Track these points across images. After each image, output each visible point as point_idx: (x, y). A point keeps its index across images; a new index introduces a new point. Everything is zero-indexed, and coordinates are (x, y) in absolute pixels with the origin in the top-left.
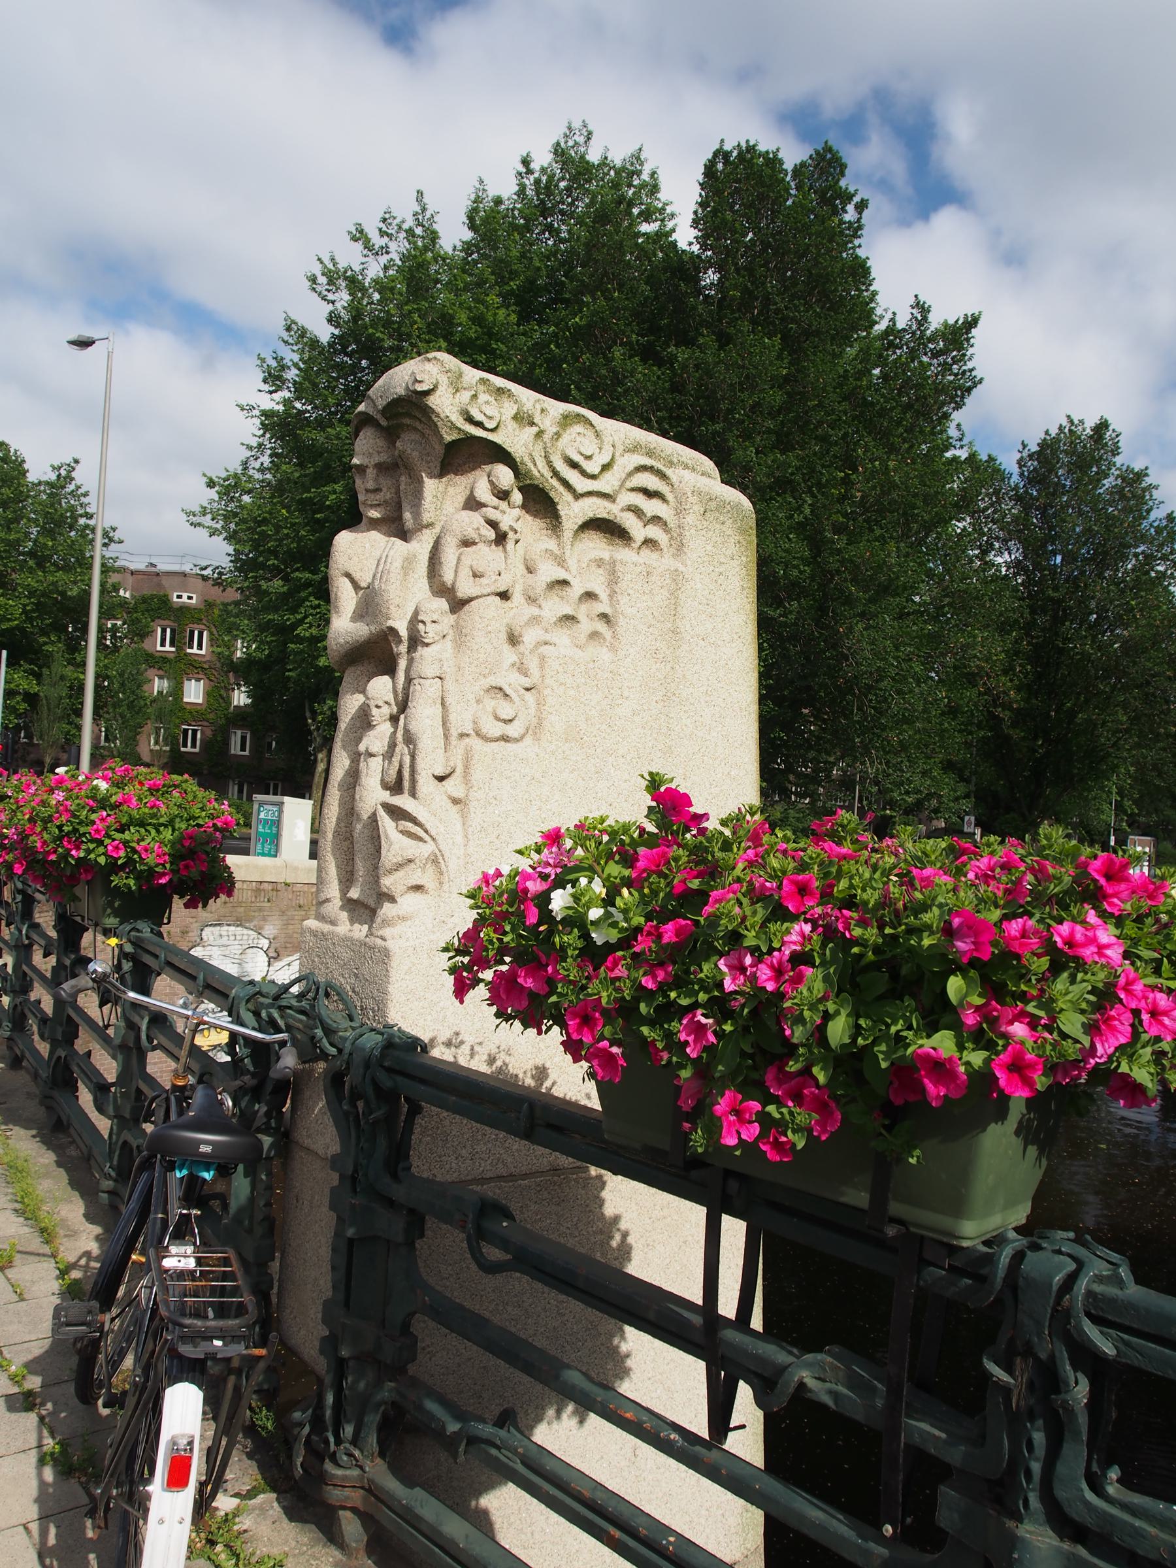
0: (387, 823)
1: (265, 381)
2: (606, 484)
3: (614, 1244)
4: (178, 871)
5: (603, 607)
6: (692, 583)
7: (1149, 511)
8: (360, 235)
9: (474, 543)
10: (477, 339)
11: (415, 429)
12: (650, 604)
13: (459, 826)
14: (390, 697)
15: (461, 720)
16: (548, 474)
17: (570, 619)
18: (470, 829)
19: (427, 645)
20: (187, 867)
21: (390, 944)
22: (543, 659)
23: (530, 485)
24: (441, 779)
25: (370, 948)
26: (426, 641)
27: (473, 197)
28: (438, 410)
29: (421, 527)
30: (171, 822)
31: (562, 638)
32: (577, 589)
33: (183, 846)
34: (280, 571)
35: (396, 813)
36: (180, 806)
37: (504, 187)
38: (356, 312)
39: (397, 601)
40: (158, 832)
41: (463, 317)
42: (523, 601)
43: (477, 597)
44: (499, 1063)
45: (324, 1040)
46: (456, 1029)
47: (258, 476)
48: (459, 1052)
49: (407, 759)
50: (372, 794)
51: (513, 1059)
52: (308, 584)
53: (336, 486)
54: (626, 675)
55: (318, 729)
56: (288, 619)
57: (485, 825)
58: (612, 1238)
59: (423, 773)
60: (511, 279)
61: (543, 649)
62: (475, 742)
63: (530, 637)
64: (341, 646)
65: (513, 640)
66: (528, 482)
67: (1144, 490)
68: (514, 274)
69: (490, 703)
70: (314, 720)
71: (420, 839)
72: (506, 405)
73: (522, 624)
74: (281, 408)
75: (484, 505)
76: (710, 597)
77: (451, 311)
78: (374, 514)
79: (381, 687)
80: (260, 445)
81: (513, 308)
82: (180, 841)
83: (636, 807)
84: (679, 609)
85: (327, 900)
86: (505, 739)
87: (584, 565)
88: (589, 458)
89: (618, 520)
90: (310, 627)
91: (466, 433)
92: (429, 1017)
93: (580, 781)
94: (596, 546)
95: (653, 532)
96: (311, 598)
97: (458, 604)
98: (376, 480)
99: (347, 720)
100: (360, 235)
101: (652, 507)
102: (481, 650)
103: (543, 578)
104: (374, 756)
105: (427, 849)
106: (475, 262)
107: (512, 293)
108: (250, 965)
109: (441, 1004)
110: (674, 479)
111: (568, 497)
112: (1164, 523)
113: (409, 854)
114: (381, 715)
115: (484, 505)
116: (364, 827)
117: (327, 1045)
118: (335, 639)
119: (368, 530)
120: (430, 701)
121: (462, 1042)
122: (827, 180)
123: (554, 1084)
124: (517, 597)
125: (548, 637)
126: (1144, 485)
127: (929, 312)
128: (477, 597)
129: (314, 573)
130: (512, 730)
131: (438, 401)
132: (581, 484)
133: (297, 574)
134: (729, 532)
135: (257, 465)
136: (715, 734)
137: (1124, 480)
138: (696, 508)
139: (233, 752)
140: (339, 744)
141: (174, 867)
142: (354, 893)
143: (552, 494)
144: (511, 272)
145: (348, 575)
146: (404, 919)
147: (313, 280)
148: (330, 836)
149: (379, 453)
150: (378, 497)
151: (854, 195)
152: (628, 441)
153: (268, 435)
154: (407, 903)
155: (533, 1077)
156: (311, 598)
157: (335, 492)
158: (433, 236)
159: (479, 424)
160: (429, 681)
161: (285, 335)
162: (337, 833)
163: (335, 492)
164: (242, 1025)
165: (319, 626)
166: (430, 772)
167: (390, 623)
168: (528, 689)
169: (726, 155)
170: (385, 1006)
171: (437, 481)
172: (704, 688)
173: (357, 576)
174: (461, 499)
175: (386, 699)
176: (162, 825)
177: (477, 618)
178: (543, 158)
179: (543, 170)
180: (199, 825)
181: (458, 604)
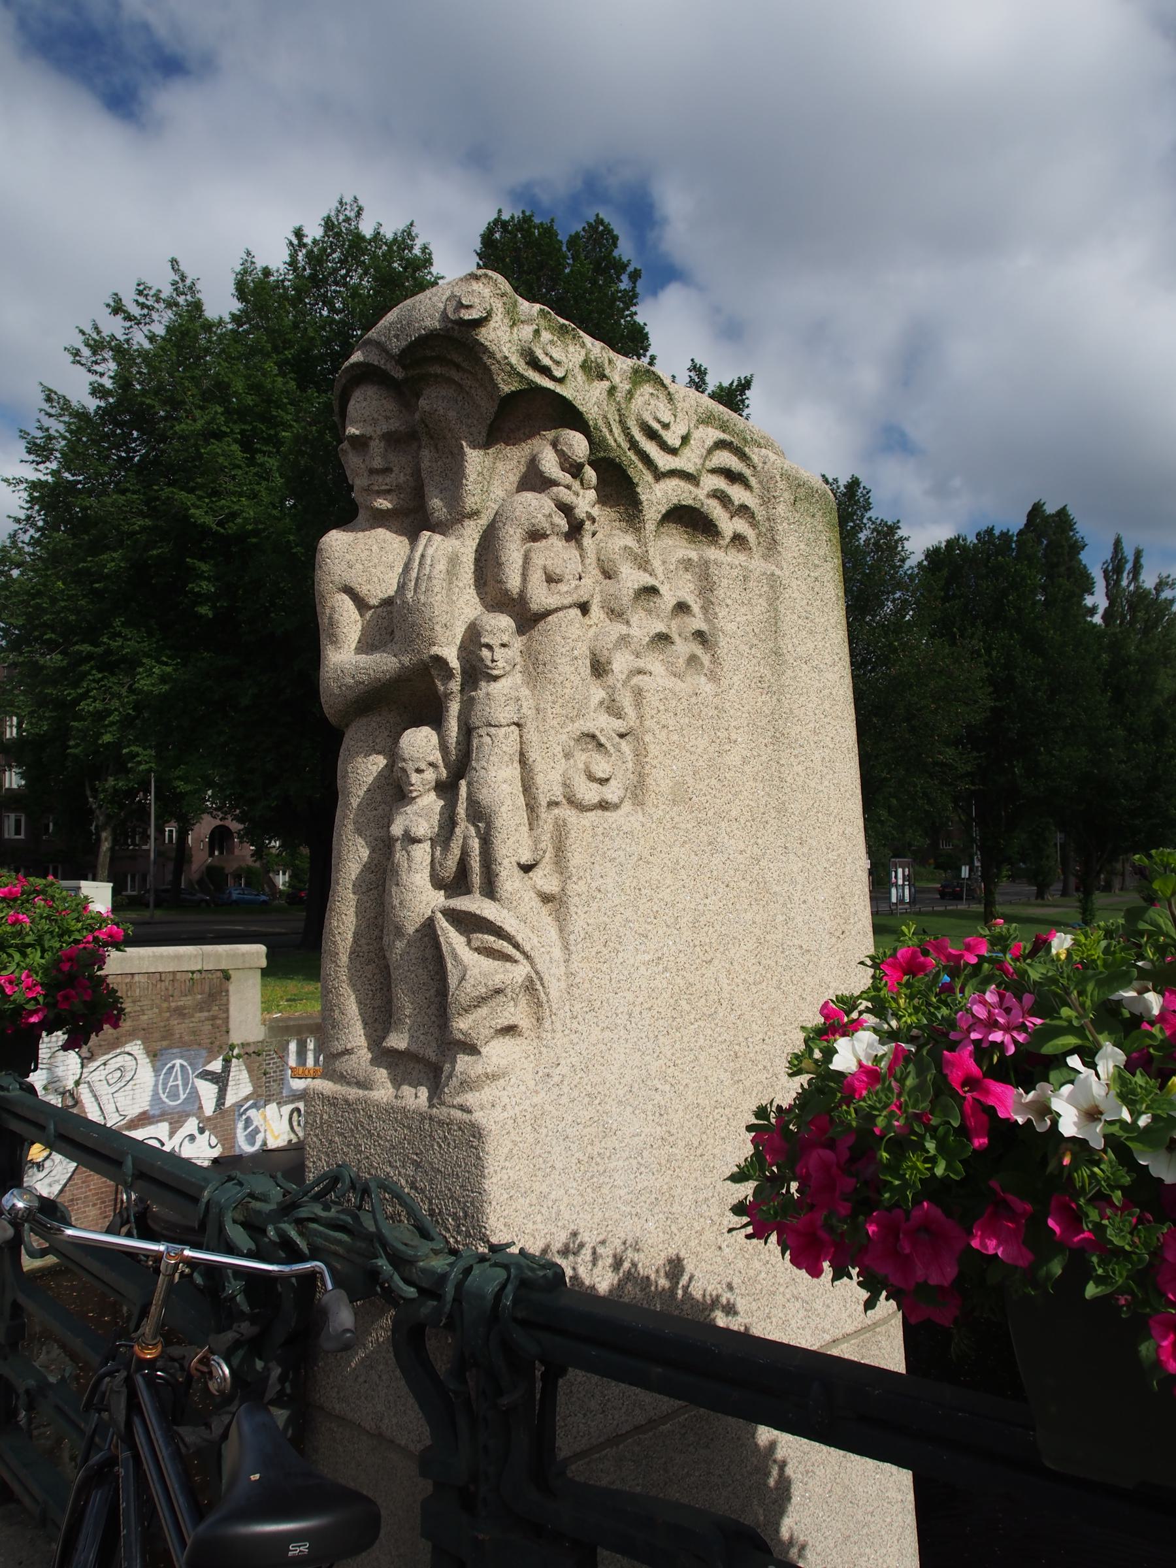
0: (453, 939)
1: (29, 452)
2: (688, 461)
3: (772, 1482)
4: (55, 1005)
5: (697, 622)
7: (903, 560)
8: (117, 308)
9: (545, 536)
10: (256, 405)
11: (450, 381)
12: (749, 617)
13: (553, 934)
14: (437, 756)
15: (549, 783)
16: (626, 446)
17: (663, 639)
18: (572, 937)
19: (496, 678)
20: (67, 998)
21: (478, 1116)
22: (638, 693)
23: (604, 459)
24: (527, 868)
25: (441, 1123)
26: (495, 672)
27: (239, 268)
28: (493, 348)
29: (459, 516)
30: (39, 941)
31: (654, 663)
32: (668, 598)
33: (60, 970)
34: (58, 645)
35: (469, 923)
36: (48, 918)
37: (274, 257)
38: (123, 381)
39: (443, 619)
40: (24, 955)
41: (239, 385)
42: (603, 616)
43: (556, 610)
44: (626, 1265)
45: (396, 1277)
46: (572, 1227)
47: (28, 549)
48: (579, 1260)
49: (475, 844)
50: (420, 896)
51: (642, 1255)
52: (90, 657)
53: (114, 555)
54: (732, 712)
55: (100, 807)
56: (69, 694)
57: (590, 929)
58: (768, 1474)
59: (506, 862)
60: (286, 349)
61: (636, 680)
62: (566, 813)
63: (621, 663)
64: (349, 688)
65: (599, 668)
66: (602, 454)
67: (896, 542)
68: (288, 344)
69: (581, 758)
70: (95, 797)
71: (508, 958)
72: (571, 349)
73: (610, 646)
74: (50, 479)
75: (555, 483)
76: (809, 608)
77: (226, 379)
78: (383, 504)
79: (421, 743)
80: (29, 518)
81: (292, 375)
82: (57, 963)
83: (754, 885)
85: (348, 1052)
86: (604, 806)
87: (672, 567)
88: (666, 426)
89: (704, 509)
90: (94, 701)
91: (530, 382)
92: (539, 1218)
93: (693, 856)
94: (674, 547)
95: (740, 525)
96: (94, 672)
97: (529, 619)
98: (384, 457)
99: (361, 793)
100: (117, 308)
101: (738, 494)
102: (568, 684)
104: (419, 841)
105: (519, 972)
106: (247, 332)
107: (286, 362)
108: (61, 1069)
109: (552, 1196)
110: (755, 459)
111: (649, 477)
112: (916, 570)
113: (497, 980)
114: (422, 782)
115: (555, 483)
116: (409, 944)
117: (401, 1284)
118: (336, 680)
119: (373, 527)
120: (506, 758)
121: (581, 1245)
122: (601, 251)
123: (691, 1278)
124: (596, 611)
125: (641, 663)
126: (896, 537)
127: (705, 374)
128: (556, 610)
129: (95, 644)
130: (612, 793)
131: (492, 336)
132: (664, 462)
133: (77, 647)
134: (820, 528)
135: (26, 538)
136: (826, 783)
137: (879, 533)
138: (786, 495)
139: (6, 836)
140: (351, 827)
141: (49, 999)
142: (398, 1041)
143: (631, 472)
144: (284, 342)
145: (349, 591)
146: (493, 1077)
147: (77, 353)
148: (344, 959)
149: (387, 418)
150: (388, 480)
151: (627, 265)
152: (700, 410)
153: (37, 507)
154: (497, 1052)
155: (667, 1275)
156: (94, 672)
157: (113, 560)
158: (197, 306)
159: (545, 371)
160: (503, 730)
161: (46, 406)
162: (354, 954)
163: (113, 560)
164: (231, 1250)
165: (104, 699)
166: (514, 859)
167: (435, 650)
168: (622, 736)
169: (504, 224)
170: (479, 1210)
171: (482, 452)
172: (811, 725)
173: (363, 590)
174: (514, 478)
175: (431, 759)
176: (29, 945)
177: (559, 639)
178: (314, 232)
179: (315, 242)
180: (76, 942)
181: (529, 619)
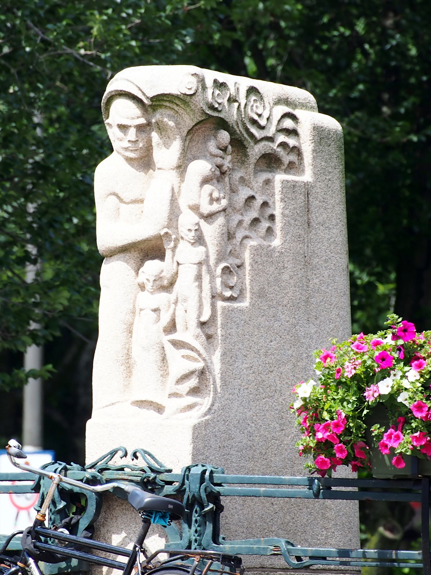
6: (315, 189)
76: (325, 196)
103: (243, 197)
143: (245, 143)
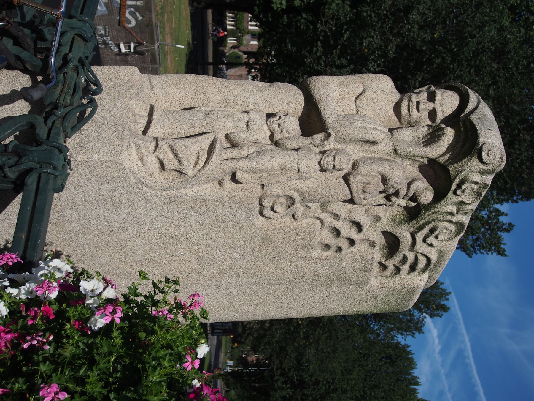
2: (421, 247)
7: (402, 334)
71: (195, 167)
76: (352, 299)
84: (345, 285)
88: (436, 237)
143: (414, 222)
